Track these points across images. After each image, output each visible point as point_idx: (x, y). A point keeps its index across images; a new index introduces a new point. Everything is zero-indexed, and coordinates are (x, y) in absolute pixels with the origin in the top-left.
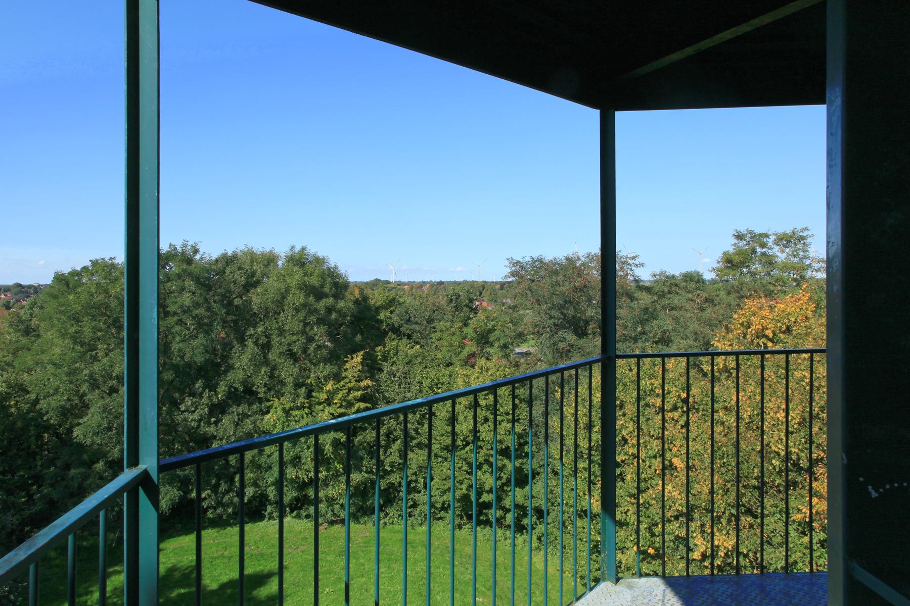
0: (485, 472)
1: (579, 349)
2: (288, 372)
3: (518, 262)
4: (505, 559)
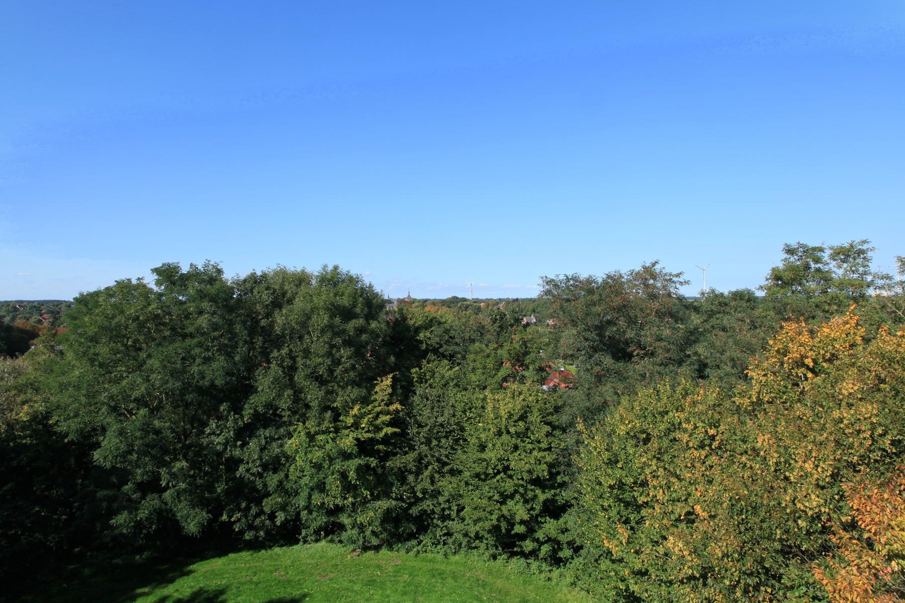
0: (517, 502)
2: (314, 395)
3: (552, 281)
4: (537, 594)
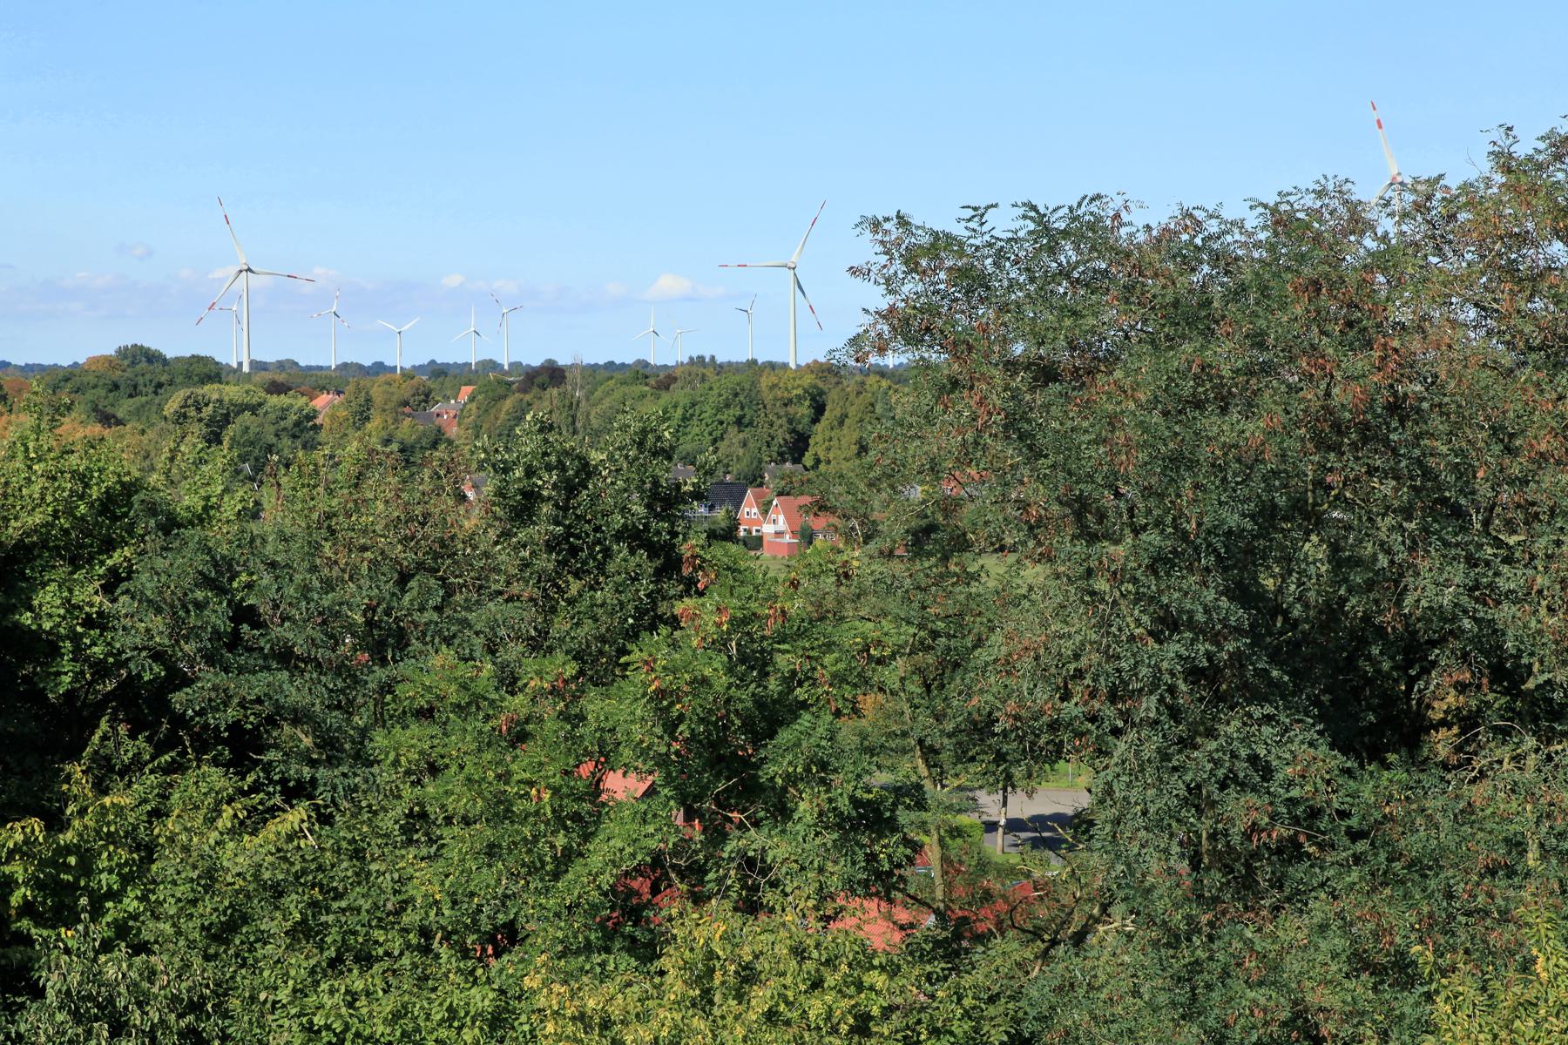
1: (1354, 835)
3: (941, 243)
